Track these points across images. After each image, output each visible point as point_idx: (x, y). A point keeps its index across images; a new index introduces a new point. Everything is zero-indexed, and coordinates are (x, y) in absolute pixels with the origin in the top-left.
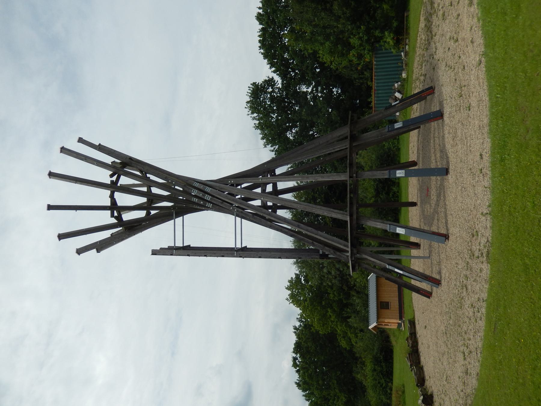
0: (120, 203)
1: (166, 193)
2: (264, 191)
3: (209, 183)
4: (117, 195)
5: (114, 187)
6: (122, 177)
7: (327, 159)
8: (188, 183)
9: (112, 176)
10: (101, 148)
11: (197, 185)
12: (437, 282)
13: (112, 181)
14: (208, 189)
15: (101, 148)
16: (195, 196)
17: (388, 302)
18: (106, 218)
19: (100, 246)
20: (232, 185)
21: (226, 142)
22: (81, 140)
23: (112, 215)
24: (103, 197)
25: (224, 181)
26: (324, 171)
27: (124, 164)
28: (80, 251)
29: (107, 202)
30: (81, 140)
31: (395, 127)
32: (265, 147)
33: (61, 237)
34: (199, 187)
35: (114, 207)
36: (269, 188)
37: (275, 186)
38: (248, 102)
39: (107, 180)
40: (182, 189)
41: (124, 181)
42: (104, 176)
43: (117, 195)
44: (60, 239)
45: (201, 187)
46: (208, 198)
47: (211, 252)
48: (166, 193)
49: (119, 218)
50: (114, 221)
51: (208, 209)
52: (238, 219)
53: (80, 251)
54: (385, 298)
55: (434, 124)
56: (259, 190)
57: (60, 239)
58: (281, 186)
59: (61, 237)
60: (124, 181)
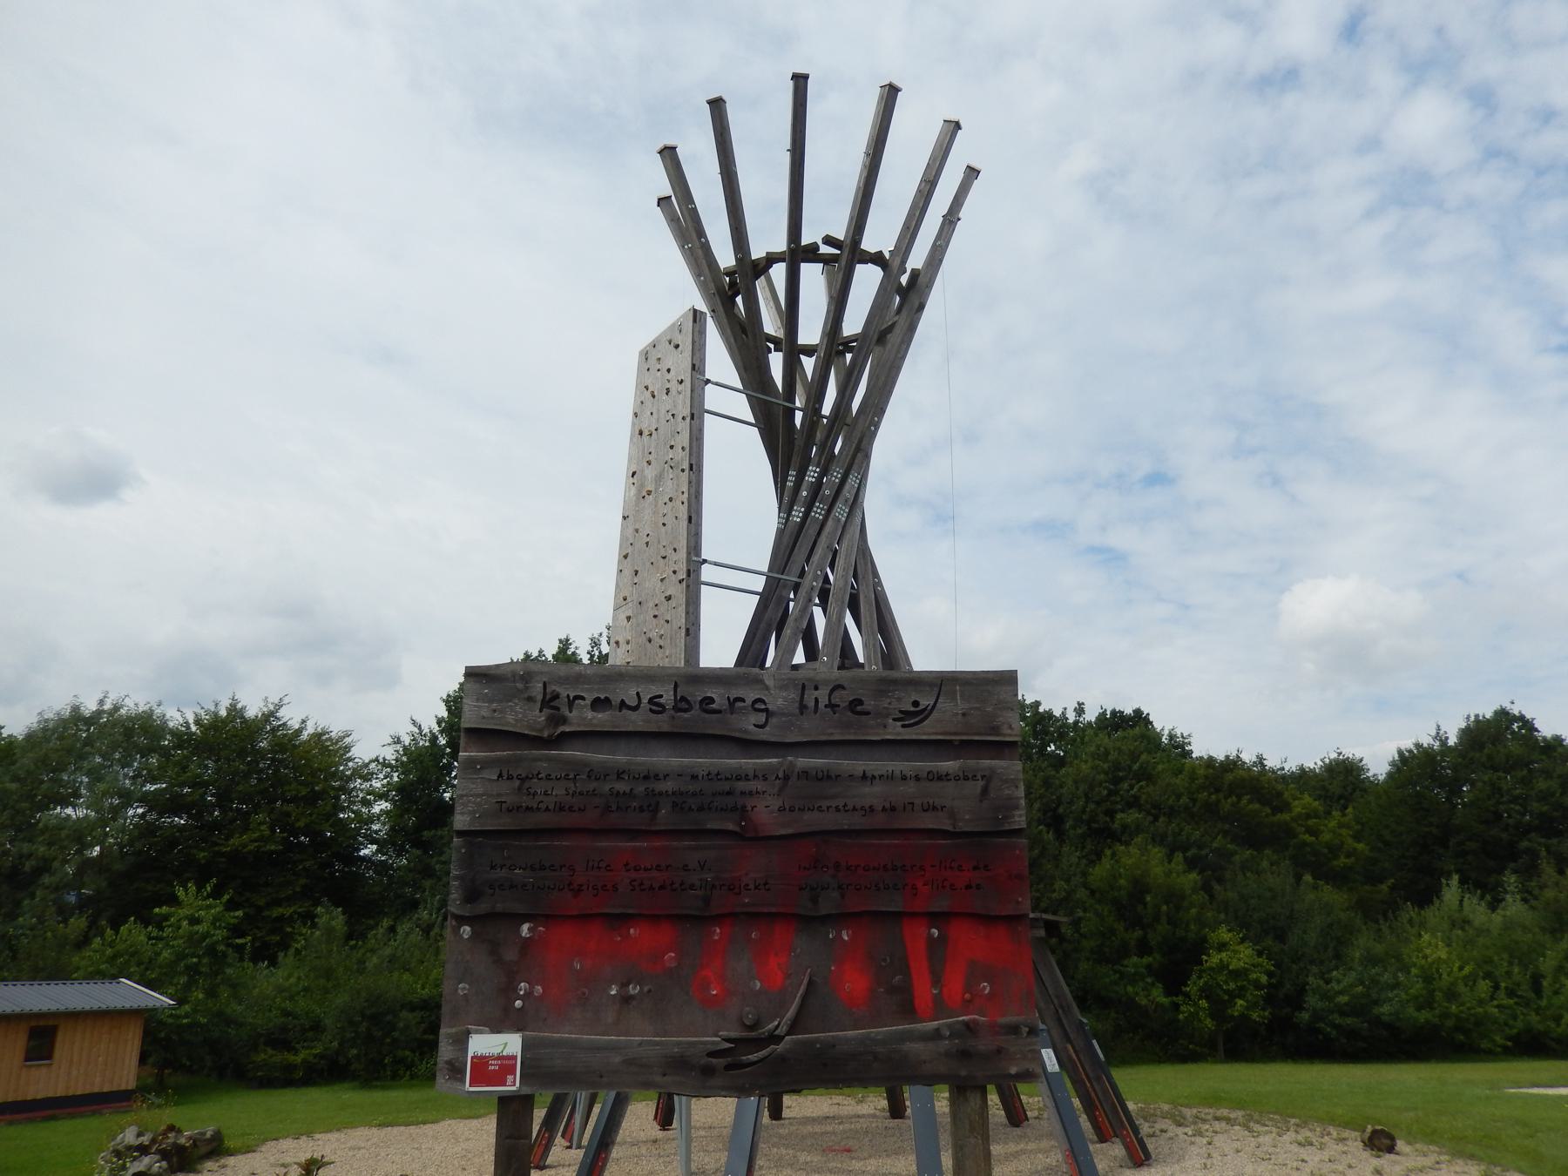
1: (827, 409)
3: (858, 520)
7: (610, 1020)
8: (859, 431)
10: (951, 219)
11: (852, 481)
14: (840, 511)
15: (951, 219)
17: (49, 1056)
18: (768, 237)
21: (985, 584)
22: (972, 173)
24: (768, 237)
25: (864, 566)
27: (906, 296)
28: (669, 154)
30: (972, 173)
34: (847, 487)
39: (869, 244)
40: (837, 451)
43: (778, 272)
44: (710, 102)
45: (848, 493)
46: (818, 512)
47: (737, 735)
48: (827, 409)
51: (785, 507)
52: (759, 583)
53: (669, 154)
54: (67, 1045)
57: (710, 102)
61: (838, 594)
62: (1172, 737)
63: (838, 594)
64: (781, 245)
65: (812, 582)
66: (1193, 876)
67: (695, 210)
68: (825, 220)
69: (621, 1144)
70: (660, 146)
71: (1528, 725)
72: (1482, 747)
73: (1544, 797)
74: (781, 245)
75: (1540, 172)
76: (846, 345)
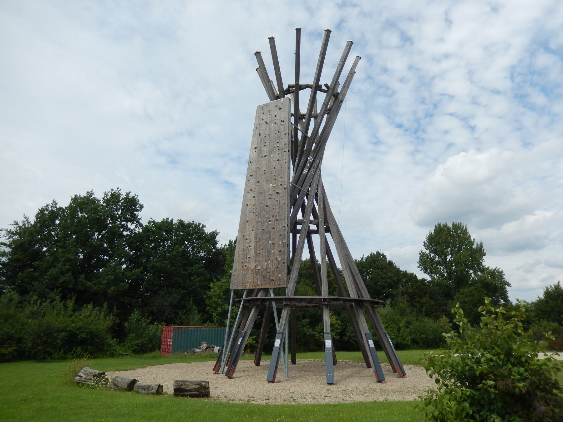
0: (301, 93)
1: (309, 134)
2: (311, 222)
4: (308, 91)
5: (317, 88)
6: (325, 95)
9: (326, 85)
10: (352, 73)
12: (229, 375)
13: (321, 86)
16: (307, 160)
19: (262, 71)
20: (317, 195)
23: (290, 87)
24: (307, 78)
26: (329, 276)
27: (336, 98)
28: (258, 54)
29: (302, 82)
31: (369, 341)
32: (481, 243)
33: (272, 40)
35: (297, 88)
36: (313, 227)
37: (314, 232)
38: (172, 221)
39: (322, 82)
40: (313, 149)
41: (321, 97)
42: (326, 79)
43: (308, 91)
45: (315, 165)
46: (305, 171)
48: (309, 134)
49: (288, 91)
50: (285, 87)
53: (258, 54)
55: (365, 364)
56: (312, 218)
58: (316, 238)
59: (272, 40)
60: (321, 97)
61: (312, 194)
62: (454, 225)
63: (312, 194)
64: (311, 82)
65: (304, 190)
66: (114, 348)
67: (267, 73)
68: (288, 80)
69: (237, 372)
70: (255, 52)
71: (384, 256)
72: (375, 263)
73: (390, 278)
74: (311, 82)
75: (380, 87)
76: (303, 116)
